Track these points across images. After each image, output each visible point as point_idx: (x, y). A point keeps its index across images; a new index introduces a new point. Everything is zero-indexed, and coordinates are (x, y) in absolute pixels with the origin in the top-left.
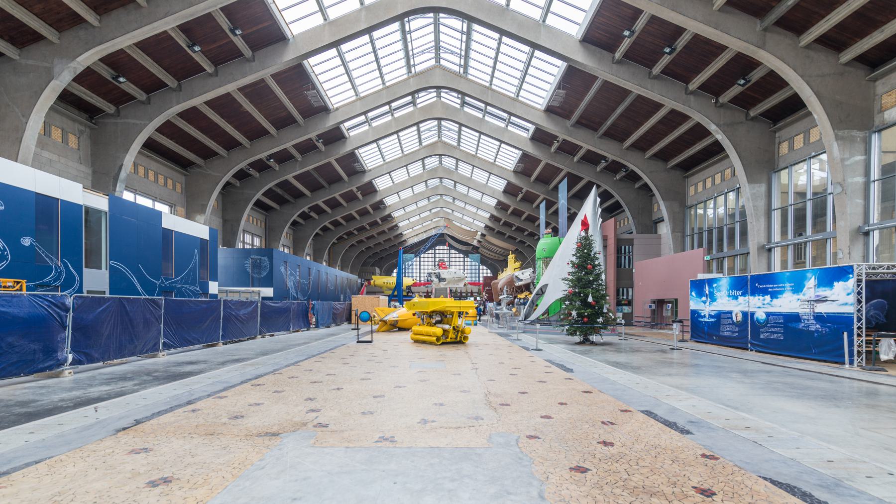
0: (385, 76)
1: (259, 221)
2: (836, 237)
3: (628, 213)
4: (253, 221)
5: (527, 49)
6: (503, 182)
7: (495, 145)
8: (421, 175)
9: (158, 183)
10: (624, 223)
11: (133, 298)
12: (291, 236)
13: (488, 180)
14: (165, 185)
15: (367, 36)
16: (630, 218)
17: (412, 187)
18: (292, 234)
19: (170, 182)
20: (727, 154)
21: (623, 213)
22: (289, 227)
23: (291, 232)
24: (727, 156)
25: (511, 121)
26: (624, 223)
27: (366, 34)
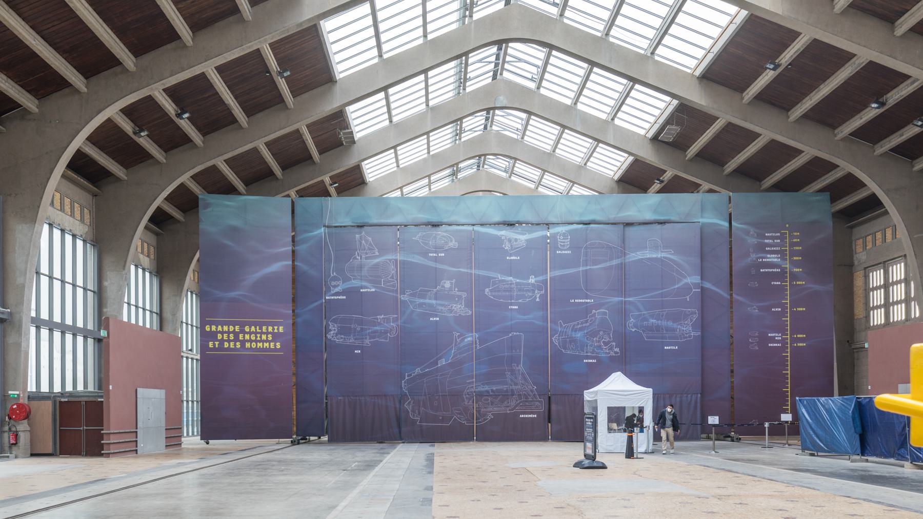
0: (378, 13)
1: (145, 245)
2: (166, 438)
3: (894, 215)
4: (72, 208)
5: (585, 65)
6: (565, 185)
7: (535, 175)
8: (420, 117)
9: (84, 222)
10: (874, 244)
11: (919, 462)
12: (152, 248)
13: (580, 93)
14: (72, 215)
15: (383, 93)
16: (902, 232)
17: (395, 147)
18: (154, 243)
19: (67, 201)
20: (886, 210)
21: (884, 218)
22: (146, 228)
23: (152, 238)
24: (886, 213)
25: (542, 183)
26: (874, 244)
27: (382, 91)
